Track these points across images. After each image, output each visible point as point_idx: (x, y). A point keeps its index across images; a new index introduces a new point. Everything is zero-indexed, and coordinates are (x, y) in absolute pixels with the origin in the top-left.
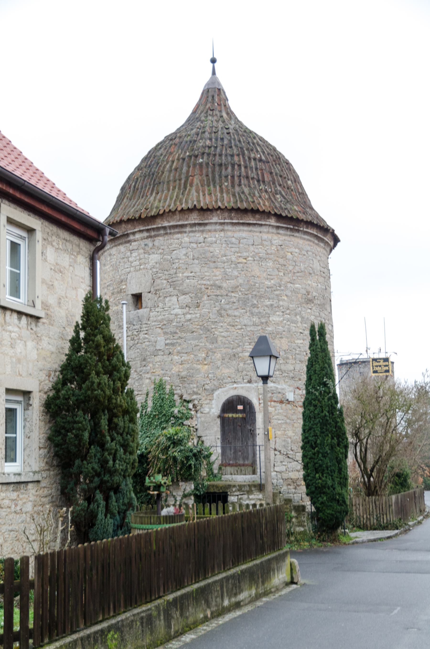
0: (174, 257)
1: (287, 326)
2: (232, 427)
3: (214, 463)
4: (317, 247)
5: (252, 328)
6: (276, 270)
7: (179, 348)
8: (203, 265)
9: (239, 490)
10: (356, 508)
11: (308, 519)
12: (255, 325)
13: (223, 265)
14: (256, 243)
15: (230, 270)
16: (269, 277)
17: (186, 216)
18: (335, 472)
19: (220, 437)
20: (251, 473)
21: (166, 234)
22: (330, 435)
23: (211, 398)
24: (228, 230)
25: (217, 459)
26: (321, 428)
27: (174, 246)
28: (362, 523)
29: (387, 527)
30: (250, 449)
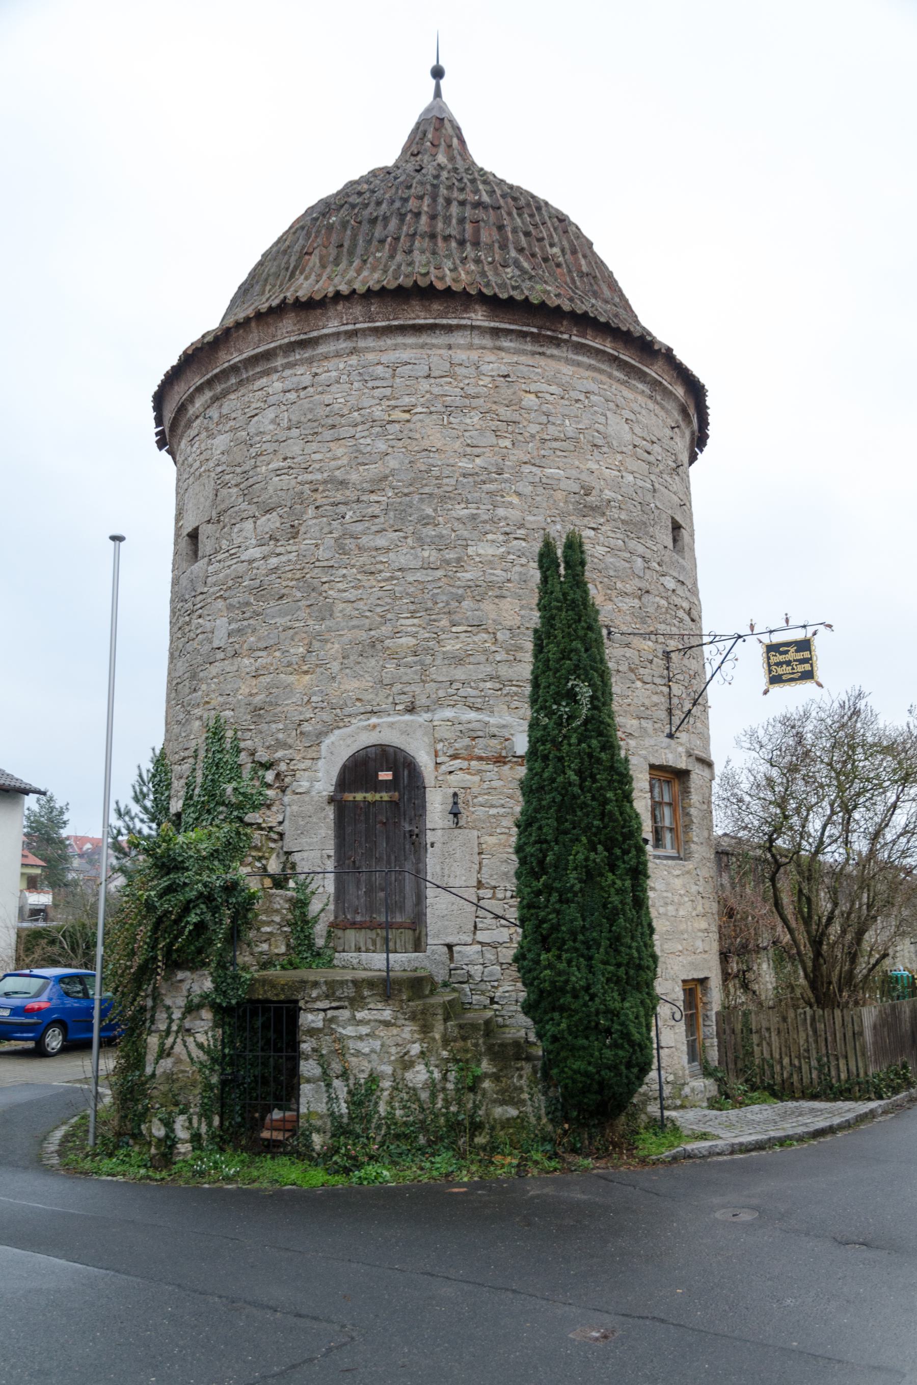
0: (252, 430)
1: (517, 569)
2: (362, 827)
3: (316, 919)
4: (623, 388)
5: (419, 576)
6: (489, 434)
7: (252, 639)
8: (310, 438)
9: (327, 997)
10: (762, 1038)
11: (533, 1082)
12: (427, 567)
13: (352, 431)
14: (435, 373)
15: (369, 441)
16: (471, 450)
17: (272, 330)
18: (599, 946)
19: (332, 853)
20: (410, 947)
21: (241, 383)
22: (584, 839)
23: (314, 755)
24: (367, 349)
25: (323, 910)
26: (558, 820)
27: (254, 406)
28: (778, 1079)
29: (849, 1090)
30: (409, 879)
